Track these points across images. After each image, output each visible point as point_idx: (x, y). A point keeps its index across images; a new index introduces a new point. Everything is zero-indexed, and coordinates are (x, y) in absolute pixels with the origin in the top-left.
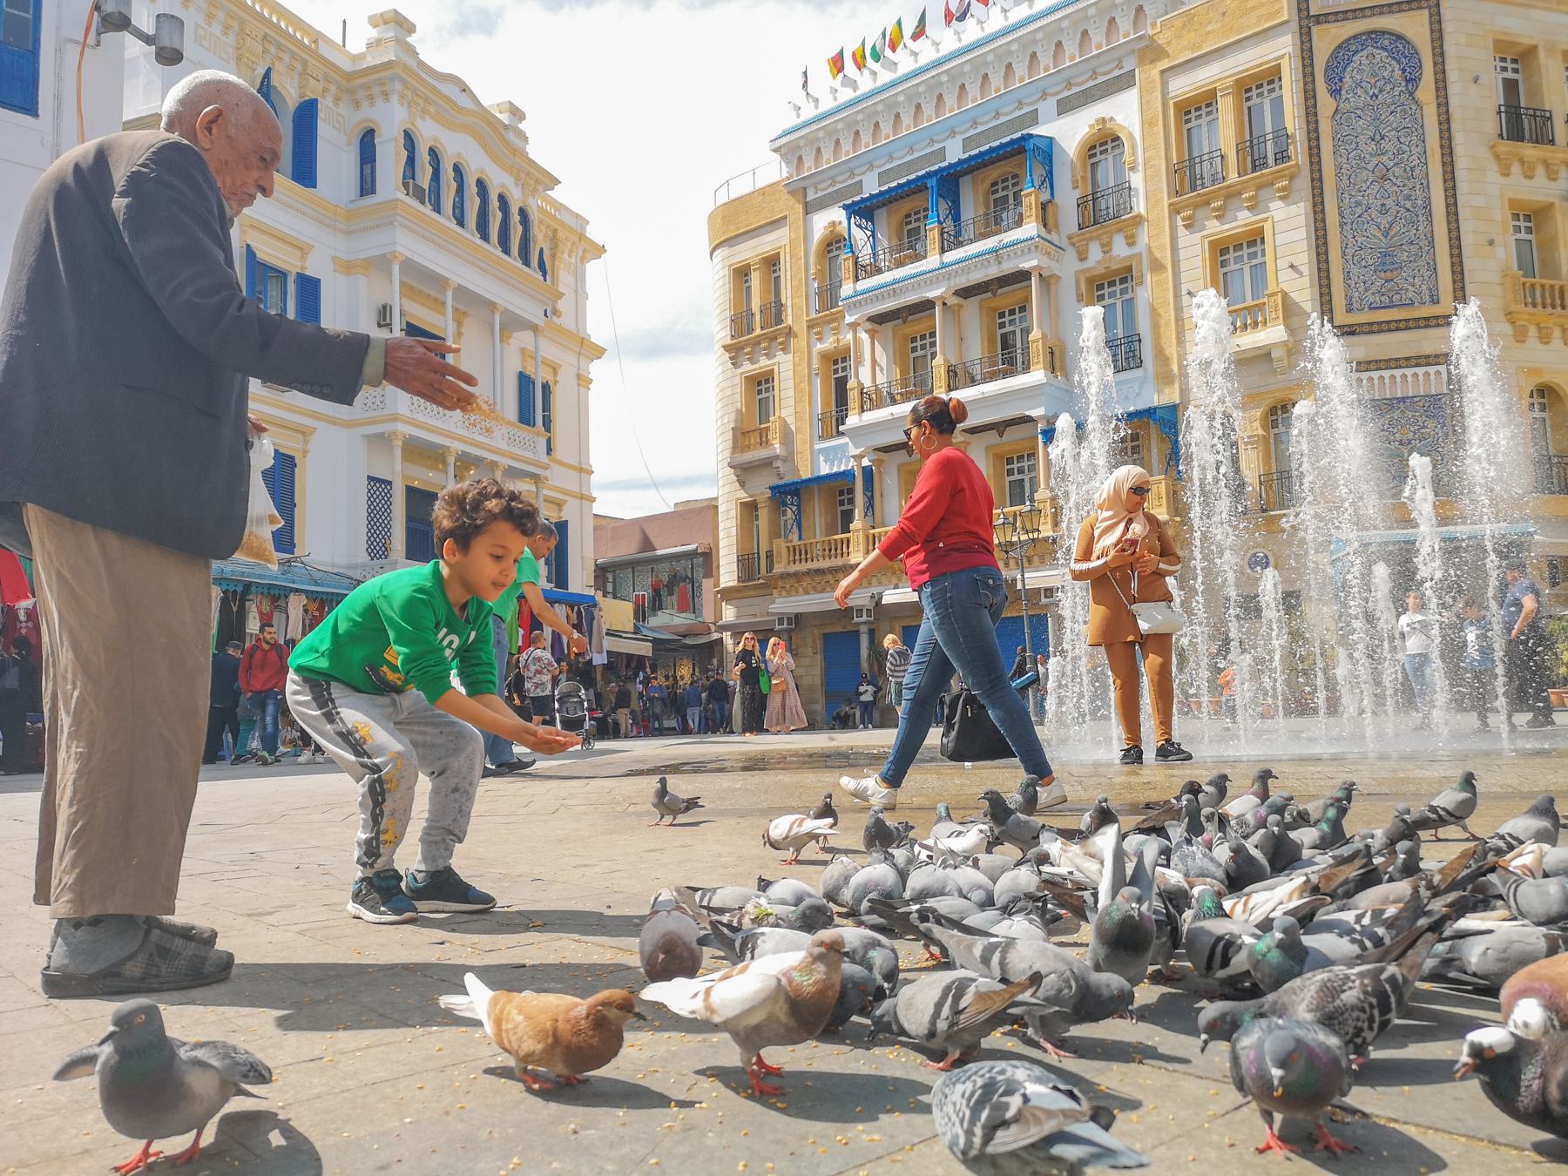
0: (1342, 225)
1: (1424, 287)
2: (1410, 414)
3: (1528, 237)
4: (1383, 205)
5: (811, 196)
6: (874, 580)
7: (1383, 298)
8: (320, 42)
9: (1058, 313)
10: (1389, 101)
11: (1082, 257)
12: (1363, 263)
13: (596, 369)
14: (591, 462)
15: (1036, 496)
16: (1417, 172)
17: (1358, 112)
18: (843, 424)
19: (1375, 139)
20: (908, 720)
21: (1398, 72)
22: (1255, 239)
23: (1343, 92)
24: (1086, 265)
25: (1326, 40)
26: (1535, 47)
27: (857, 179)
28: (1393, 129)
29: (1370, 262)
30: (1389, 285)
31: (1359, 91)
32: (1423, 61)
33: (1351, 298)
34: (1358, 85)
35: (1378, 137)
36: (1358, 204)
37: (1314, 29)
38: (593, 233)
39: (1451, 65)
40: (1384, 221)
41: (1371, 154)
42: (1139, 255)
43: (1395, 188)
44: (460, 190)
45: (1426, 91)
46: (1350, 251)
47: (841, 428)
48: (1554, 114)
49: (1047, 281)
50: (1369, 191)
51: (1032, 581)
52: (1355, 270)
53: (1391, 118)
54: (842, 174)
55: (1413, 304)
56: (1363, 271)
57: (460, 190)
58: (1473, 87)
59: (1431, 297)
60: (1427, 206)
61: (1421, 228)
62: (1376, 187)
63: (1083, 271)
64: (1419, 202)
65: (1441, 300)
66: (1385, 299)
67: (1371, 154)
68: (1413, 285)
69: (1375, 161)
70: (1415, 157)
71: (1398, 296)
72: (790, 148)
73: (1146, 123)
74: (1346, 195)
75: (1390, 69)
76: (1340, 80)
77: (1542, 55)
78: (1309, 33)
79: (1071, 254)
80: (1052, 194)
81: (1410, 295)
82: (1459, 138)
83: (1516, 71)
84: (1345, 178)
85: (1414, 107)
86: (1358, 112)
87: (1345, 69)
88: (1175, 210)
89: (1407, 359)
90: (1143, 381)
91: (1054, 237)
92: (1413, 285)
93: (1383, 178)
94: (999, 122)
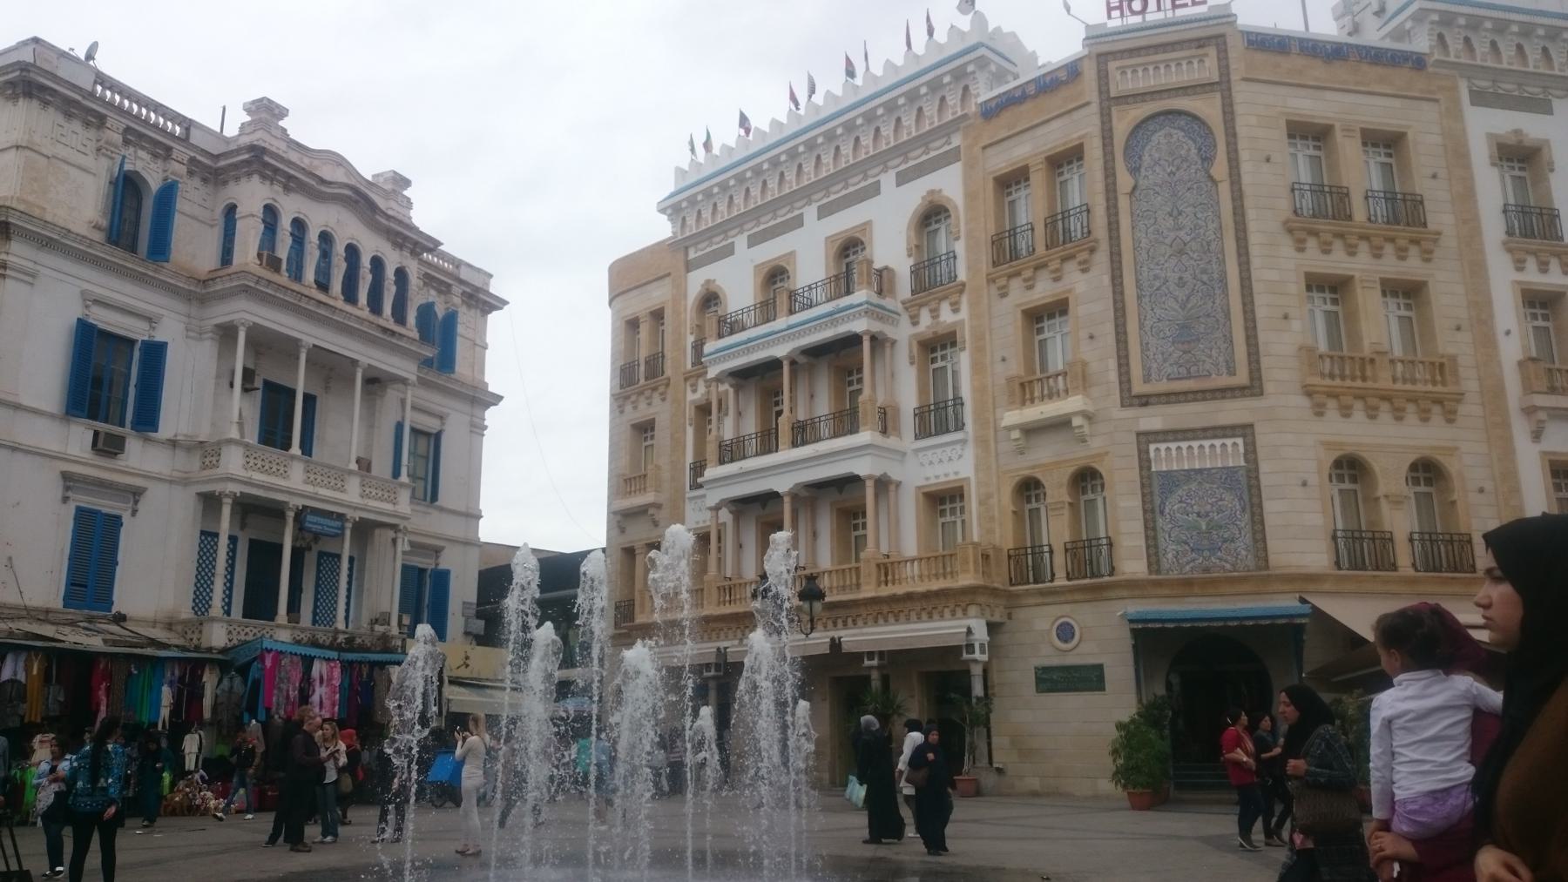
0: (1139, 298)
1: (1221, 359)
2: (1208, 486)
3: (1334, 308)
4: (1181, 278)
5: (692, 255)
6: (714, 635)
7: (1181, 370)
8: (192, 128)
9: (893, 375)
11: (915, 324)
12: (1162, 335)
14: (481, 507)
15: (862, 555)
16: (1213, 247)
17: (1157, 189)
18: (702, 475)
19: (1175, 214)
20: (896, 803)
21: (1194, 151)
22: (1059, 308)
23: (1143, 170)
25: (1123, 124)
27: (730, 241)
28: (1189, 206)
29: (1168, 334)
30: (1187, 357)
31: (1157, 169)
32: (1218, 140)
33: (1150, 368)
34: (1157, 163)
35: (1175, 213)
36: (1156, 277)
37: (1114, 110)
38: (496, 288)
39: (1242, 144)
40: (1181, 294)
42: (962, 322)
43: (1192, 262)
44: (326, 255)
45: (1220, 169)
46: (1148, 323)
47: (700, 480)
49: (877, 341)
50: (1166, 265)
53: (1188, 194)
55: (1210, 375)
57: (326, 255)
61: (1218, 301)
62: (1173, 261)
63: (915, 336)
64: (1216, 276)
65: (1237, 372)
66: (1183, 371)
67: (1169, 230)
68: (1210, 357)
69: (1172, 235)
70: (1210, 232)
72: (674, 208)
73: (970, 196)
74: (1145, 269)
75: (1186, 147)
76: (1140, 158)
77: (1338, 135)
78: (1109, 115)
79: (905, 320)
81: (1207, 366)
82: (1251, 214)
86: (1157, 189)
87: (1143, 147)
88: (991, 280)
89: (1205, 430)
91: (888, 302)
92: (1210, 357)
93: (1181, 252)
94: (847, 192)
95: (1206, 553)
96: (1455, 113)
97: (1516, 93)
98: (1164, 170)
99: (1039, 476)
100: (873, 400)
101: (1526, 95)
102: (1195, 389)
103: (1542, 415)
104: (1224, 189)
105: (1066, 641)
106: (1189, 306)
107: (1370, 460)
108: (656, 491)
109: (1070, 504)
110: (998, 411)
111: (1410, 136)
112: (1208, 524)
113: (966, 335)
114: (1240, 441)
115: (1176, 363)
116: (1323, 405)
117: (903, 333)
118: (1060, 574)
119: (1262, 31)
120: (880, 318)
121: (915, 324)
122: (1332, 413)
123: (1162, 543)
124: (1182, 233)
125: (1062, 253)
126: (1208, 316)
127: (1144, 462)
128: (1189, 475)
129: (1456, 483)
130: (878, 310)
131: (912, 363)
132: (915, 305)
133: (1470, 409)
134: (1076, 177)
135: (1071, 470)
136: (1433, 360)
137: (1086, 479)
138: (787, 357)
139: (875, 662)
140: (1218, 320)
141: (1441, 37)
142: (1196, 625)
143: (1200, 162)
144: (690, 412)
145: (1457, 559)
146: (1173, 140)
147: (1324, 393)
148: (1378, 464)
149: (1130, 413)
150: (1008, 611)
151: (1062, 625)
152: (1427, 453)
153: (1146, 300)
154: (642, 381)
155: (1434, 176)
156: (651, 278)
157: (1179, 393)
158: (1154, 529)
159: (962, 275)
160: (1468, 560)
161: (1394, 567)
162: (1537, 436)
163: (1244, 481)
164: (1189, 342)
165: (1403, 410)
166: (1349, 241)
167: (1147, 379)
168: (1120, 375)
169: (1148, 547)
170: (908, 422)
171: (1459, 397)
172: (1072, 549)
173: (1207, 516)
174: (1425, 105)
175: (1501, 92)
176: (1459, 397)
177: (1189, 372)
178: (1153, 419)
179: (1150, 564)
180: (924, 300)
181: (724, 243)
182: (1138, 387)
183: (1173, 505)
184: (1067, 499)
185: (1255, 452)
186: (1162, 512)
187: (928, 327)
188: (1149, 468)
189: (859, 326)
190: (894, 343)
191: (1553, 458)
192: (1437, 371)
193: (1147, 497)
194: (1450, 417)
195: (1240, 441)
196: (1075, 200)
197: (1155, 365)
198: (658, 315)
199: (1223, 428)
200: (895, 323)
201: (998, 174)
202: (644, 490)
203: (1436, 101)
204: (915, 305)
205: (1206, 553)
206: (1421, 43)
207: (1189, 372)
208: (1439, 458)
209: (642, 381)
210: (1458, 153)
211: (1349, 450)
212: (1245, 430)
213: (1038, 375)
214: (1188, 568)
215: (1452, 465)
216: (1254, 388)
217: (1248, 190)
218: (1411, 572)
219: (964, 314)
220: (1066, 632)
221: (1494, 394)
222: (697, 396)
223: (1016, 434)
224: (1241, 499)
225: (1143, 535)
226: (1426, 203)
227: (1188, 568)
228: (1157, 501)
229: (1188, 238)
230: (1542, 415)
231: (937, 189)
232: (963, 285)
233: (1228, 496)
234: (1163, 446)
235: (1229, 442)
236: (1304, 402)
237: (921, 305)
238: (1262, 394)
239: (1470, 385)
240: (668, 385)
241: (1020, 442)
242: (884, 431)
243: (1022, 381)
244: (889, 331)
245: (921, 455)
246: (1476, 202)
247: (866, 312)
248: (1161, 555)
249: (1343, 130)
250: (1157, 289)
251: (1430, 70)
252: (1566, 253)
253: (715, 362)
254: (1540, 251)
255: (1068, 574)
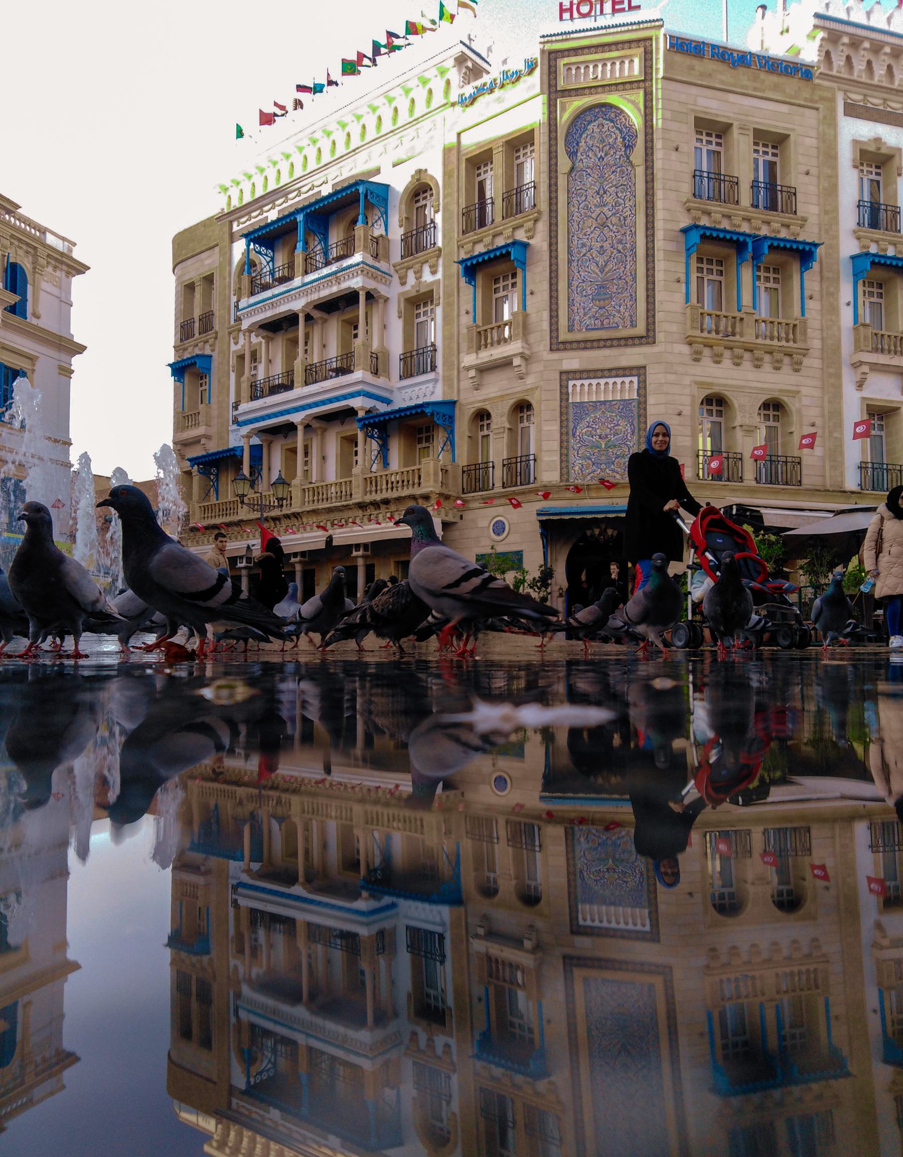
1: (627, 314)
4: (602, 247)
7: (596, 322)
10: (612, 162)
12: (584, 293)
13: (77, 362)
16: (628, 221)
19: (600, 193)
23: (579, 154)
24: (408, 287)
26: (731, 125)
29: (589, 292)
30: (601, 312)
35: (602, 192)
36: (584, 245)
40: (601, 260)
41: (596, 206)
42: (438, 281)
43: (611, 234)
46: (575, 283)
48: (741, 179)
50: (592, 235)
51: (338, 540)
52: (578, 298)
53: (613, 177)
54: (255, 211)
55: (618, 326)
56: (584, 299)
58: (674, 154)
59: (631, 322)
60: (633, 248)
61: (628, 267)
62: (597, 232)
63: (403, 293)
64: (628, 246)
67: (596, 206)
68: (619, 312)
69: (598, 211)
70: (627, 209)
71: (607, 321)
73: (447, 174)
74: (575, 238)
76: (577, 144)
77: (735, 131)
80: (386, 230)
82: (659, 194)
83: (774, 155)
84: (575, 224)
85: (630, 169)
87: (581, 136)
89: (610, 370)
90: (436, 381)
91: (383, 265)
92: (619, 312)
93: (604, 225)
95: (603, 466)
96: (832, 123)
97: (881, 108)
98: (596, 155)
99: (488, 408)
100: (367, 344)
101: (889, 109)
102: (605, 338)
103: (865, 369)
104: (640, 171)
105: (499, 535)
106: (607, 270)
107: (732, 399)
108: (206, 425)
109: (509, 429)
110: (461, 355)
111: (792, 138)
112: (606, 445)
113: (440, 293)
114: (635, 379)
115: (594, 316)
116: (700, 353)
117: (394, 292)
118: (498, 484)
119: (683, 36)
120: (375, 278)
121: (403, 284)
122: (707, 361)
123: (572, 459)
124: (605, 209)
125: (514, 223)
126: (620, 278)
127: (564, 395)
128: (597, 405)
129: (795, 418)
130: (372, 270)
131: (400, 317)
132: (403, 268)
133: (812, 362)
134: (529, 160)
135: (512, 401)
136: (788, 322)
137: (522, 407)
138: (302, 310)
139: (361, 553)
140: (627, 282)
141: (828, 54)
142: (585, 516)
143: (623, 149)
144: (233, 361)
145: (789, 476)
146: (604, 130)
147: (700, 343)
148: (737, 401)
149: (556, 356)
150: (460, 514)
151: (496, 522)
152: (776, 395)
153: (575, 264)
154: (197, 335)
155: (807, 173)
156: (204, 248)
157: (594, 341)
158: (567, 449)
159: (440, 244)
160: (796, 477)
161: (741, 479)
162: (860, 385)
163: (635, 410)
164: (604, 300)
165: (761, 360)
166: (735, 222)
167: (571, 329)
168: (551, 324)
169: (561, 461)
170: (396, 367)
171: (805, 352)
172: (509, 464)
173: (606, 437)
174: (808, 112)
175: (869, 105)
176: (805, 352)
177: (602, 324)
178: (572, 361)
179: (561, 475)
180: (410, 263)
181: (260, 217)
182: (564, 336)
183: (582, 429)
184: (507, 425)
185: (645, 388)
186: (574, 435)
187: (413, 287)
188: (568, 399)
189: (356, 283)
190: (387, 300)
191: (871, 403)
192: (791, 331)
193: (563, 424)
194: (797, 367)
195: (635, 379)
196: (529, 176)
197: (577, 318)
198: (209, 280)
199: (624, 369)
200: (388, 284)
201: (469, 156)
202: (197, 425)
203: (817, 109)
204: (403, 268)
205: (603, 466)
206: (810, 54)
207: (602, 324)
208: (785, 399)
209: (197, 335)
210: (829, 154)
211: (716, 389)
212: (640, 371)
213: (494, 324)
214: (589, 477)
215: (792, 404)
216: (648, 338)
217: (659, 174)
218: (754, 483)
219: (439, 276)
220: (499, 528)
221: (831, 354)
222: (239, 347)
223: (472, 373)
224: (632, 424)
225: (559, 452)
226: (798, 194)
227: (589, 477)
228: (571, 425)
229: (610, 213)
230: (865, 369)
231: (424, 168)
232: (440, 250)
233: (622, 423)
234: (578, 383)
235: (627, 380)
236: (685, 349)
237: (408, 268)
238: (654, 342)
239: (815, 344)
240: (216, 338)
241: (475, 380)
242: (376, 373)
243: (479, 330)
244: (382, 289)
245: (403, 392)
246: (837, 196)
247: (362, 271)
248: (570, 467)
249: (741, 128)
250: (584, 255)
251: (817, 81)
252: (900, 243)
253: (249, 315)
254: (883, 240)
255: (503, 483)
